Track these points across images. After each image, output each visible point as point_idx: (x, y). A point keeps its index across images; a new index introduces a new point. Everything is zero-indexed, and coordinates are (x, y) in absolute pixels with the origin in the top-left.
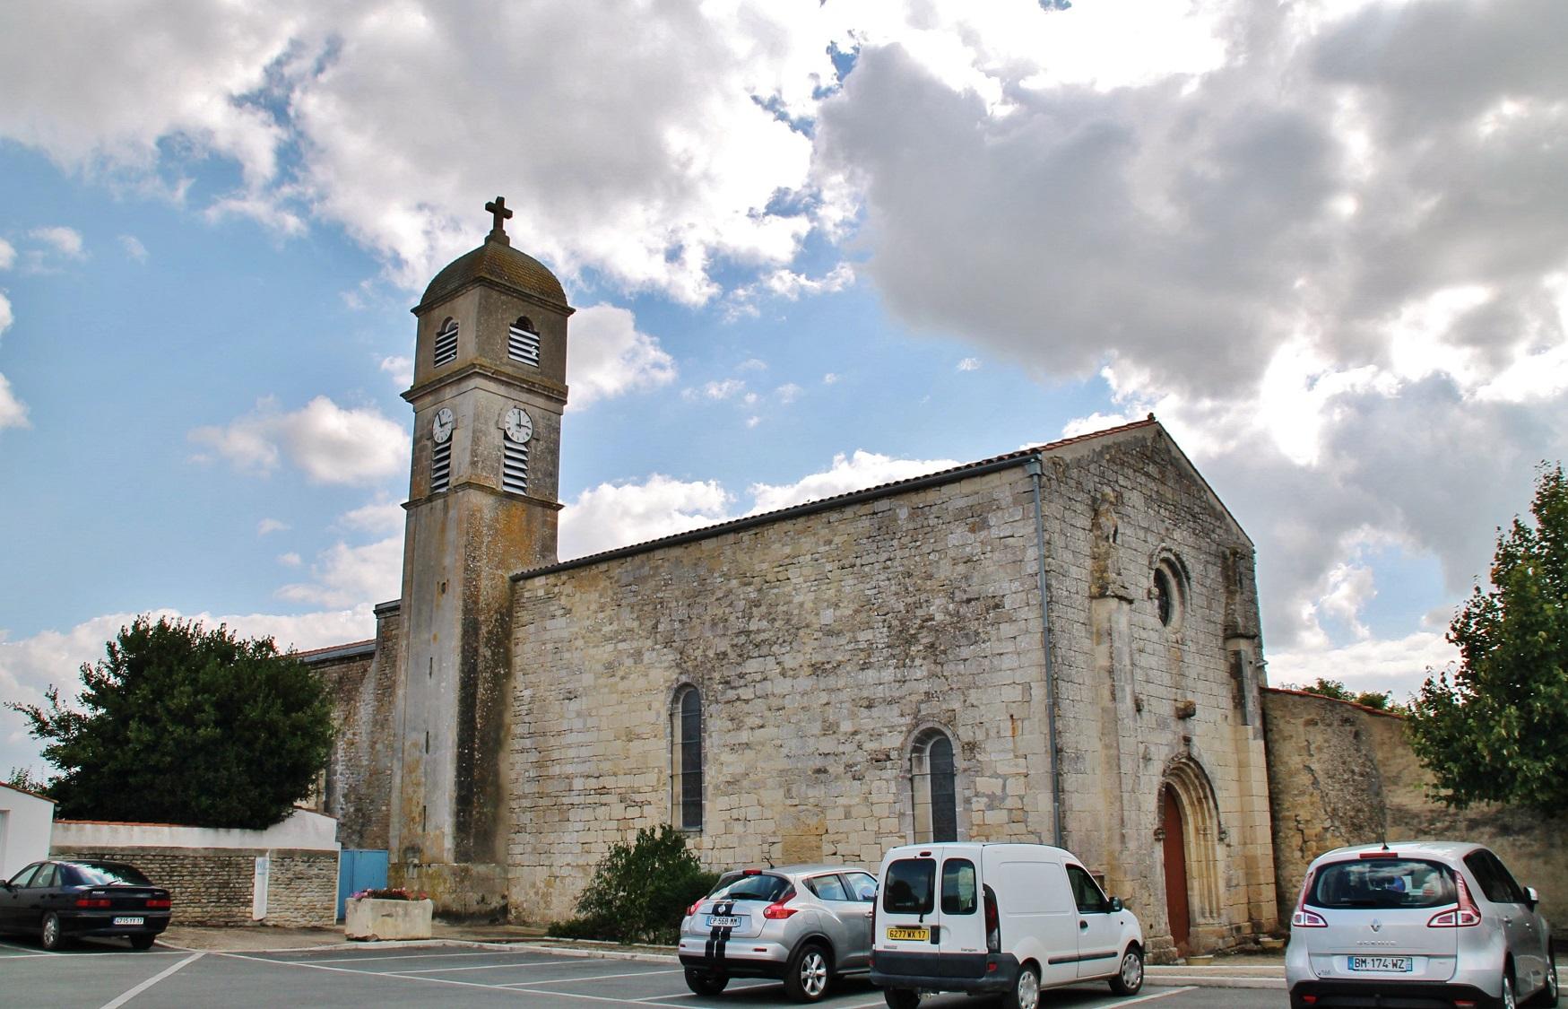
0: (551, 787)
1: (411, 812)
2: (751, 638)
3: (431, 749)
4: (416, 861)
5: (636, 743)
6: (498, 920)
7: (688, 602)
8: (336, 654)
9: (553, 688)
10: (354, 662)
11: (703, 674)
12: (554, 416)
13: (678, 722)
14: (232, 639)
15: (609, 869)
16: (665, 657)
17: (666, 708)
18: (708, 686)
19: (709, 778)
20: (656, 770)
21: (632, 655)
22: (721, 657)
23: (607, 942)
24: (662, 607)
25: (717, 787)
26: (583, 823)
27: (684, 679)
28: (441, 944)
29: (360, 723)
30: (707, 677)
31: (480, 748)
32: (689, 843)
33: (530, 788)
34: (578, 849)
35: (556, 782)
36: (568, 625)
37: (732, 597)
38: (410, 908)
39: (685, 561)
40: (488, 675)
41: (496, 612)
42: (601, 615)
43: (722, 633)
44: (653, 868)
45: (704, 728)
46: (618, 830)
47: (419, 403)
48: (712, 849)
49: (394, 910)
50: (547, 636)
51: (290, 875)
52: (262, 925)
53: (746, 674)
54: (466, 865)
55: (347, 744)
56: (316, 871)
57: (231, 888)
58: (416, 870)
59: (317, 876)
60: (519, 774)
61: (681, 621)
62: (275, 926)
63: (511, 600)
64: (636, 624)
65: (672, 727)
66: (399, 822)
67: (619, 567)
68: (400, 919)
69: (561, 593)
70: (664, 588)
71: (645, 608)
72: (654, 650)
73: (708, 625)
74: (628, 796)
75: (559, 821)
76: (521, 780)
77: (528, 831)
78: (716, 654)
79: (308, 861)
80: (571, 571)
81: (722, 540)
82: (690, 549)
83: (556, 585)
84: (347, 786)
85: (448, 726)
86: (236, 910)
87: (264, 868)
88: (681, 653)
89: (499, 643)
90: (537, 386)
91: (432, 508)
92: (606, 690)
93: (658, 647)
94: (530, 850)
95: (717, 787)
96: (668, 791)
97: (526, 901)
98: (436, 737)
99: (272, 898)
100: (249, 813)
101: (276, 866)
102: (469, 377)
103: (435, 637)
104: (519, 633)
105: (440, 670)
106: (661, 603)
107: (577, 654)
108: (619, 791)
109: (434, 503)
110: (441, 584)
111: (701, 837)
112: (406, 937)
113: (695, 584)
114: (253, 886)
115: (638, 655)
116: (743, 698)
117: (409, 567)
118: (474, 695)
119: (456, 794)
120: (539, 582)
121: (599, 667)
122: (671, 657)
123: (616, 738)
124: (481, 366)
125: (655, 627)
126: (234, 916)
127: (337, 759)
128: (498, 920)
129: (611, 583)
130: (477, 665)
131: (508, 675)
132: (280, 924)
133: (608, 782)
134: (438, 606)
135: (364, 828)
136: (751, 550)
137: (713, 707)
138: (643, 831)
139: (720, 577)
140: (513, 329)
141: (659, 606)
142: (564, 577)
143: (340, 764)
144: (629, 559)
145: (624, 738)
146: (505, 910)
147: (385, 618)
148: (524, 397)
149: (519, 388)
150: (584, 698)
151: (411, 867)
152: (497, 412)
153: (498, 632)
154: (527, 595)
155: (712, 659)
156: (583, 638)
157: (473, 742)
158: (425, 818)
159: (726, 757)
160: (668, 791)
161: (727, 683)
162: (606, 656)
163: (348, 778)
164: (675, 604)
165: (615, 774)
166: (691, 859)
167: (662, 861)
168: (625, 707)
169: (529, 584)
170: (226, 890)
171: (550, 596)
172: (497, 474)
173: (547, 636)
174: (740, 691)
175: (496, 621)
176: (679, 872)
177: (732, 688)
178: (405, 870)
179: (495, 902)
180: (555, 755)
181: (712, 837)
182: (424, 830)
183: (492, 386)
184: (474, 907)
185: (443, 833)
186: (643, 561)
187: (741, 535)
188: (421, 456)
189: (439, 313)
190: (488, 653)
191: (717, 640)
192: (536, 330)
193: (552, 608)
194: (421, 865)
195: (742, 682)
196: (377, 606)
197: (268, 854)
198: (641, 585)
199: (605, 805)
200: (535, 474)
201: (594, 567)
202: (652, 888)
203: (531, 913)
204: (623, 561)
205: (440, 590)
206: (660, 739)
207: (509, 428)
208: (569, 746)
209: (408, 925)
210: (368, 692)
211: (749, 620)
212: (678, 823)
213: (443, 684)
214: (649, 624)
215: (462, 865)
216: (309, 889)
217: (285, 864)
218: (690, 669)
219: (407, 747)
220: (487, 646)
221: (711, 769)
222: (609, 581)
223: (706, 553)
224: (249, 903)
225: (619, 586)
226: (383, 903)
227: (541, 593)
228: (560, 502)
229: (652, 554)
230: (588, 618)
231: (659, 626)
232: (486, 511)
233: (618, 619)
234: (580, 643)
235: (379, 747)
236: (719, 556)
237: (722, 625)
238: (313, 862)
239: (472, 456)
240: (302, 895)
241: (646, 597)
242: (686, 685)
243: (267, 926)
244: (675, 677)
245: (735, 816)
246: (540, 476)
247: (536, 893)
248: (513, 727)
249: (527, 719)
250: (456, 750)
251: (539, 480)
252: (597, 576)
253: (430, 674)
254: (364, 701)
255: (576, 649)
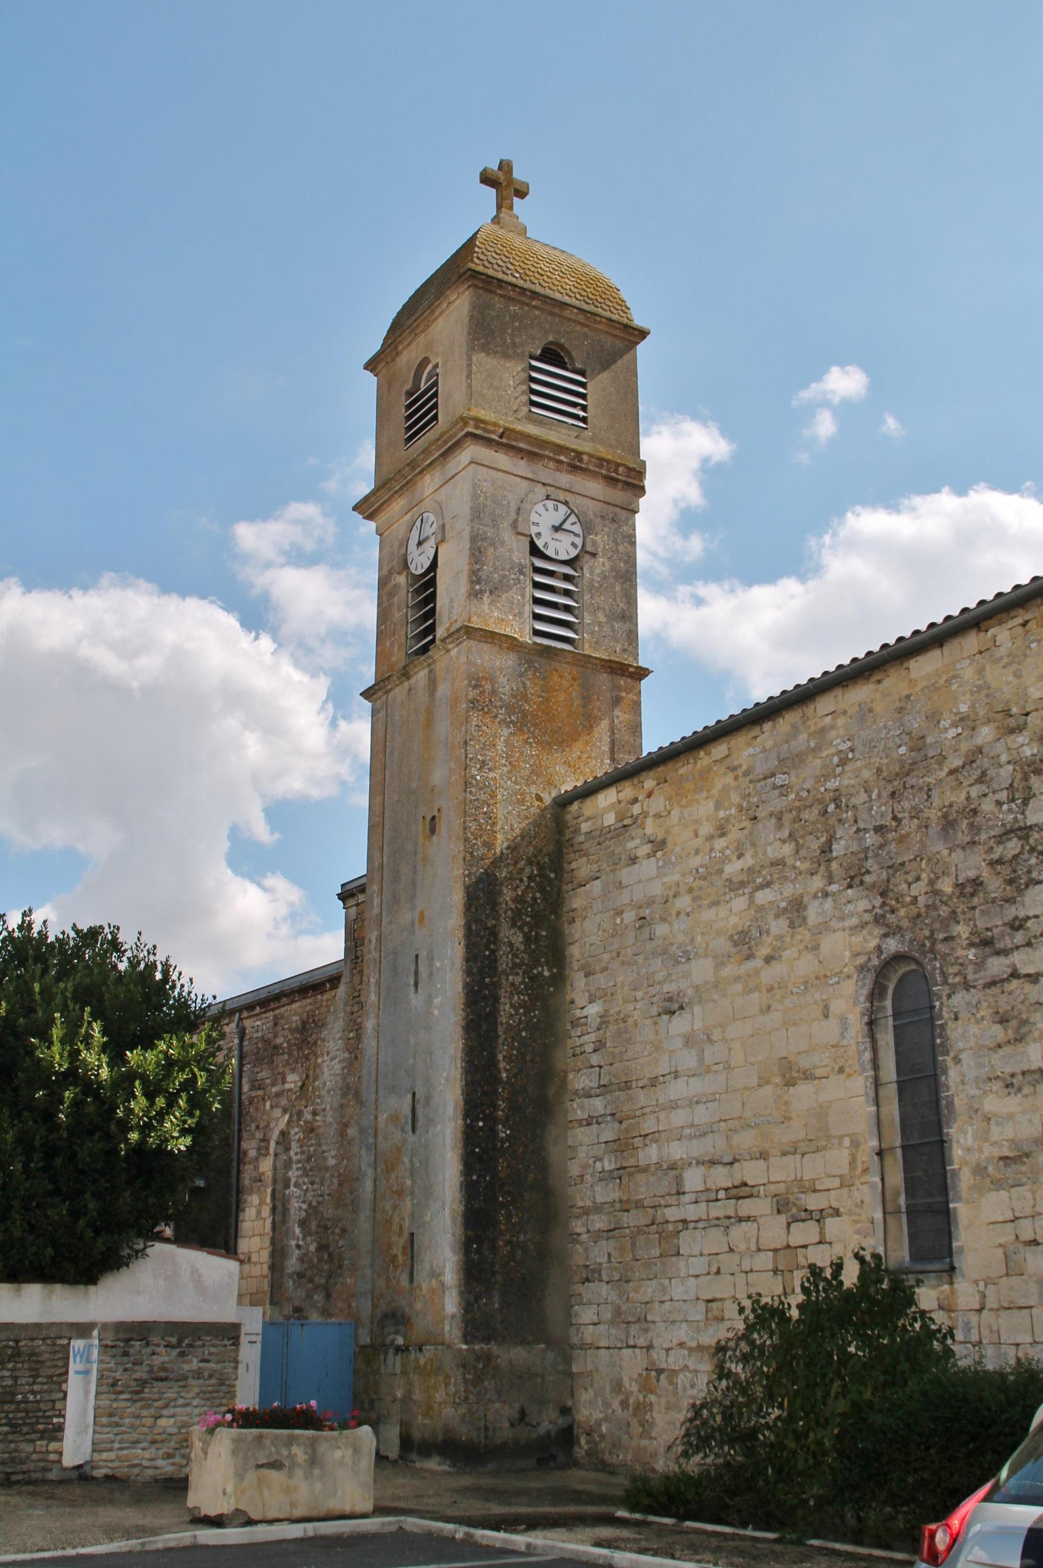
0: (644, 1189)
1: (390, 1246)
2: (1031, 841)
3: (419, 1124)
4: (400, 1341)
5: (803, 1089)
6: (553, 1457)
7: (890, 788)
8: (295, 984)
9: (639, 994)
10: (322, 993)
11: (932, 932)
12: (622, 514)
13: (887, 1038)
14: (43, 935)
15: (745, 1359)
16: (850, 907)
17: (858, 1010)
18: (944, 957)
19: (960, 1152)
20: (847, 1142)
21: (785, 910)
22: (968, 890)
23: (749, 1532)
24: (838, 807)
25: (979, 1170)
26: (705, 1259)
27: (893, 945)
28: (393, 1528)
29: (323, 1093)
30: (941, 936)
31: (507, 1118)
32: (927, 1297)
33: (605, 1193)
34: (697, 1313)
35: (652, 1179)
36: (661, 872)
37: (983, 762)
38: (322, 1448)
39: (878, 708)
40: (519, 979)
41: (530, 863)
42: (720, 843)
43: (968, 839)
44: (846, 1357)
45: (942, 1045)
46: (775, 1271)
47: (383, 516)
48: (980, 1311)
49: (285, 1452)
50: (624, 898)
51: (141, 1373)
52: (82, 1475)
53: (1028, 918)
54: (485, 1347)
55: (304, 1131)
56: (195, 1364)
57: (18, 1403)
58: (399, 1357)
59: (198, 1374)
60: (585, 1167)
61: (879, 829)
62: (107, 1477)
63: (558, 841)
64: (787, 849)
65: (875, 1050)
66: (372, 1265)
67: (749, 745)
68: (299, 1473)
69: (645, 814)
70: (839, 770)
71: (805, 815)
72: (826, 895)
73: (935, 829)
74: (792, 1198)
75: (661, 1255)
76: (588, 1177)
77: (605, 1278)
78: (957, 885)
79: (179, 1345)
80: (661, 769)
81: (952, 648)
82: (886, 683)
83: (635, 801)
84: (304, 1206)
85: (447, 1079)
86: (29, 1448)
87: (89, 1361)
88: (883, 894)
89: (539, 920)
90: (585, 457)
91: (410, 690)
92: (739, 987)
93: (834, 888)
94: (608, 1316)
95: (979, 1170)
96: (872, 1186)
97: (605, 1419)
98: (428, 1099)
99: (105, 1420)
100: (50, 1251)
101: (113, 1356)
102: (457, 445)
103: (422, 918)
104: (577, 901)
105: (431, 975)
106: (835, 800)
107: (680, 925)
108: (772, 1188)
109: (413, 681)
110: (429, 817)
111: (951, 1283)
112: (314, 1513)
113: (903, 750)
114: (65, 1398)
115: (796, 909)
116: (1024, 971)
117: (378, 800)
118: (491, 1018)
119: (463, 1208)
120: (607, 799)
121: (722, 944)
122: (863, 905)
123: (763, 1082)
124: (478, 421)
125: (827, 849)
126: (22, 1462)
127: (290, 1158)
128: (553, 1457)
129: (736, 778)
130: (496, 961)
131: (559, 979)
132: (119, 1473)
133: (752, 1172)
134: (424, 860)
135: (332, 1281)
136: (1015, 659)
137: (960, 999)
138: (815, 1271)
139: (954, 725)
140: (534, 363)
141: (831, 808)
142: (649, 783)
143: (295, 1166)
144: (767, 726)
145: (778, 1080)
146: (567, 1436)
147: (357, 905)
148: (565, 479)
149: (551, 464)
150: (697, 1009)
151: (391, 1351)
152: (513, 507)
153: (534, 899)
154: (585, 827)
155: (950, 898)
156: (690, 890)
157: (495, 1107)
158: (412, 1258)
159: (994, 1103)
160: (872, 1186)
161: (986, 943)
162: (734, 920)
163: (307, 1189)
164: (863, 797)
165: (763, 1156)
166: (931, 1335)
167: (866, 1341)
168: (776, 1016)
169: (589, 807)
170: (6, 1407)
171: (626, 822)
172: (520, 614)
173: (624, 898)
174: (1017, 958)
175: (530, 878)
176: (905, 1366)
177: (998, 953)
178: (382, 1357)
179: (548, 1422)
180: (649, 1125)
181: (976, 1282)
182: (411, 1281)
183: (502, 459)
184: (504, 1432)
185: (443, 1284)
186: (794, 726)
187: (990, 633)
188: (392, 605)
189: (408, 357)
190: (518, 939)
191: (958, 856)
192: (578, 365)
193: (630, 845)
194: (407, 1349)
195: (1019, 938)
196: (342, 886)
197: (95, 1333)
198: (793, 772)
199: (748, 1219)
200: (593, 613)
201: (702, 754)
202: (842, 1406)
203: (616, 1446)
204: (756, 731)
205: (427, 831)
206: (849, 1075)
207: (539, 534)
208: (673, 1106)
209: (318, 1486)
210: (333, 1039)
211: (1026, 802)
212: (899, 1254)
213: (437, 1001)
214: (814, 845)
215: (477, 1347)
216: (181, 1401)
217: (132, 1351)
218: (905, 924)
219: (381, 1125)
220: (514, 925)
221: (965, 1133)
222: (731, 775)
223: (921, 685)
224: (56, 1432)
225: (751, 781)
226: (261, 1436)
227: (610, 819)
228: (642, 663)
229: (811, 707)
230: (697, 852)
231: (834, 847)
232: (502, 680)
233: (754, 845)
234: (684, 902)
235: (352, 1132)
236: (948, 682)
237: (965, 822)
238: (190, 1346)
239: (472, 582)
240: (165, 1412)
241: (805, 794)
242: (899, 958)
243: (94, 1478)
244: (873, 943)
245: (1027, 1235)
246: (602, 618)
247: (624, 1404)
248: (571, 1076)
249: (595, 1059)
250: (460, 1122)
251: (600, 624)
252: (708, 769)
253: (416, 985)
254: (328, 1053)
255: (678, 914)
